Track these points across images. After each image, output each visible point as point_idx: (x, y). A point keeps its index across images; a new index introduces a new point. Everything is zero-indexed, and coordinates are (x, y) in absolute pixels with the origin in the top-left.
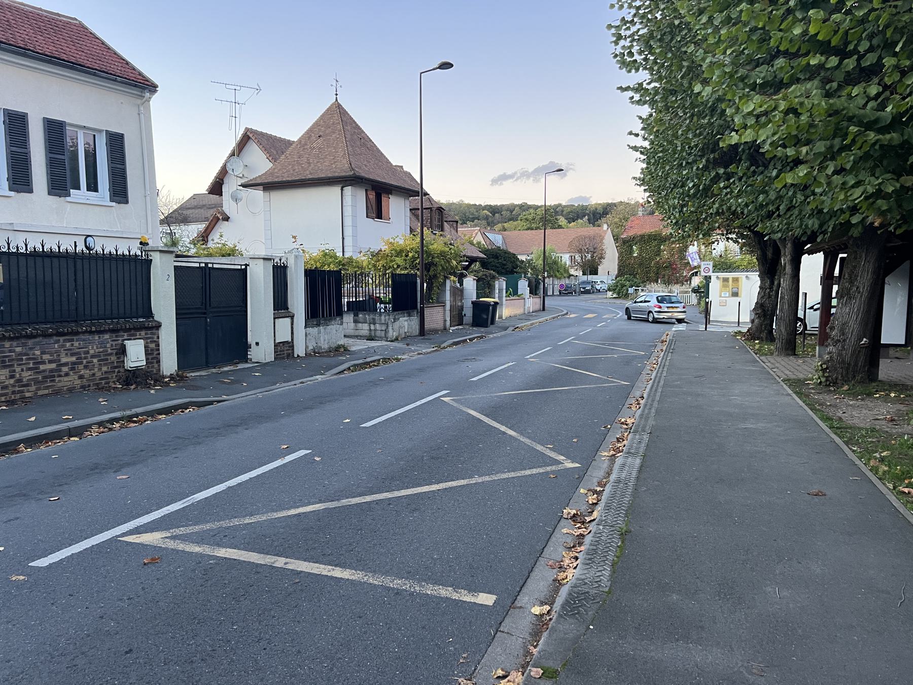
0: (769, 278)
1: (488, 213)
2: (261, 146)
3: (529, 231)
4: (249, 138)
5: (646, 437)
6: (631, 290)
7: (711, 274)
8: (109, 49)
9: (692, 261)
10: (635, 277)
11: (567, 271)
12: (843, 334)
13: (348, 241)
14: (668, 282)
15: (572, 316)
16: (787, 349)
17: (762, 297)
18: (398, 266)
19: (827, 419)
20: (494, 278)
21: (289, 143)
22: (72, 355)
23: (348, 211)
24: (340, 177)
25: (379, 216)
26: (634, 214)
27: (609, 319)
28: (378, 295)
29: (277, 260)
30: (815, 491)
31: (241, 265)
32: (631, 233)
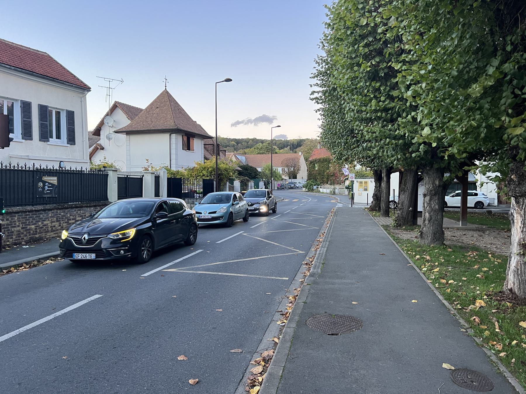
0: (379, 182)
1: (235, 143)
2: (124, 111)
3: (259, 155)
4: (117, 106)
5: (328, 243)
6: (315, 187)
7: (354, 179)
8: (64, 69)
9: (345, 172)
10: (316, 181)
11: (280, 176)
12: (403, 206)
13: (173, 162)
14: (333, 183)
15: (287, 200)
16: (385, 214)
17: (376, 191)
18: (204, 175)
19: (393, 237)
20: (248, 181)
21: (142, 110)
22: (80, 216)
23: (173, 146)
24: (170, 129)
25: (189, 149)
26: (315, 146)
27: (305, 202)
28: (195, 190)
29: (156, 174)
30: (381, 253)
31: (125, 175)
32: (314, 158)
